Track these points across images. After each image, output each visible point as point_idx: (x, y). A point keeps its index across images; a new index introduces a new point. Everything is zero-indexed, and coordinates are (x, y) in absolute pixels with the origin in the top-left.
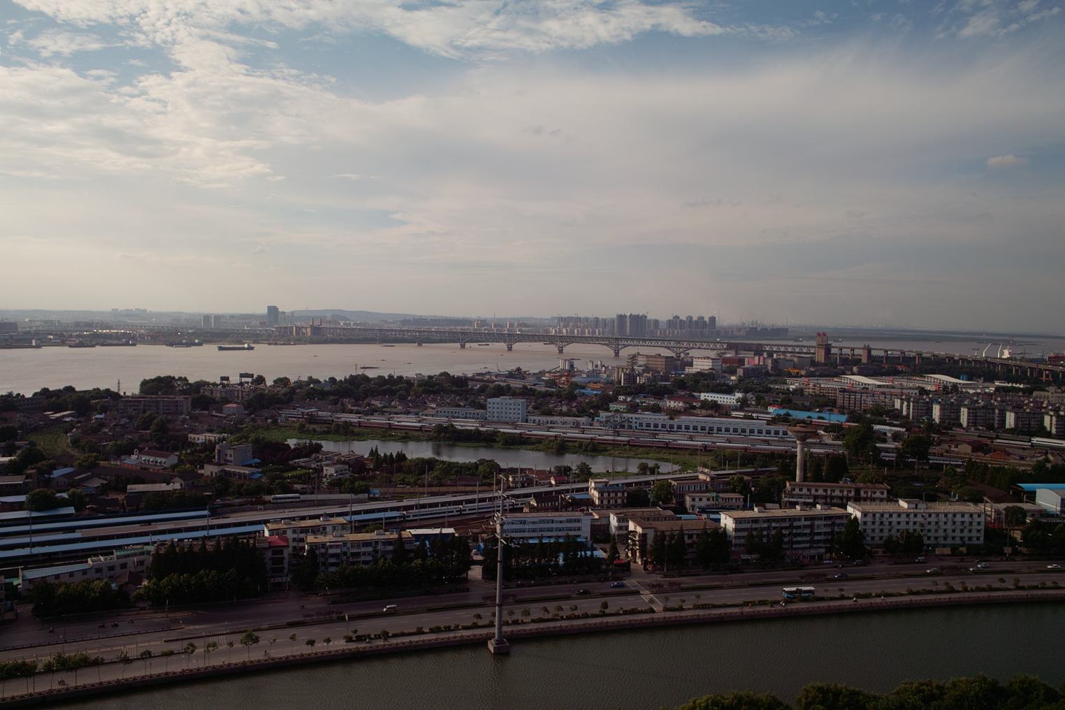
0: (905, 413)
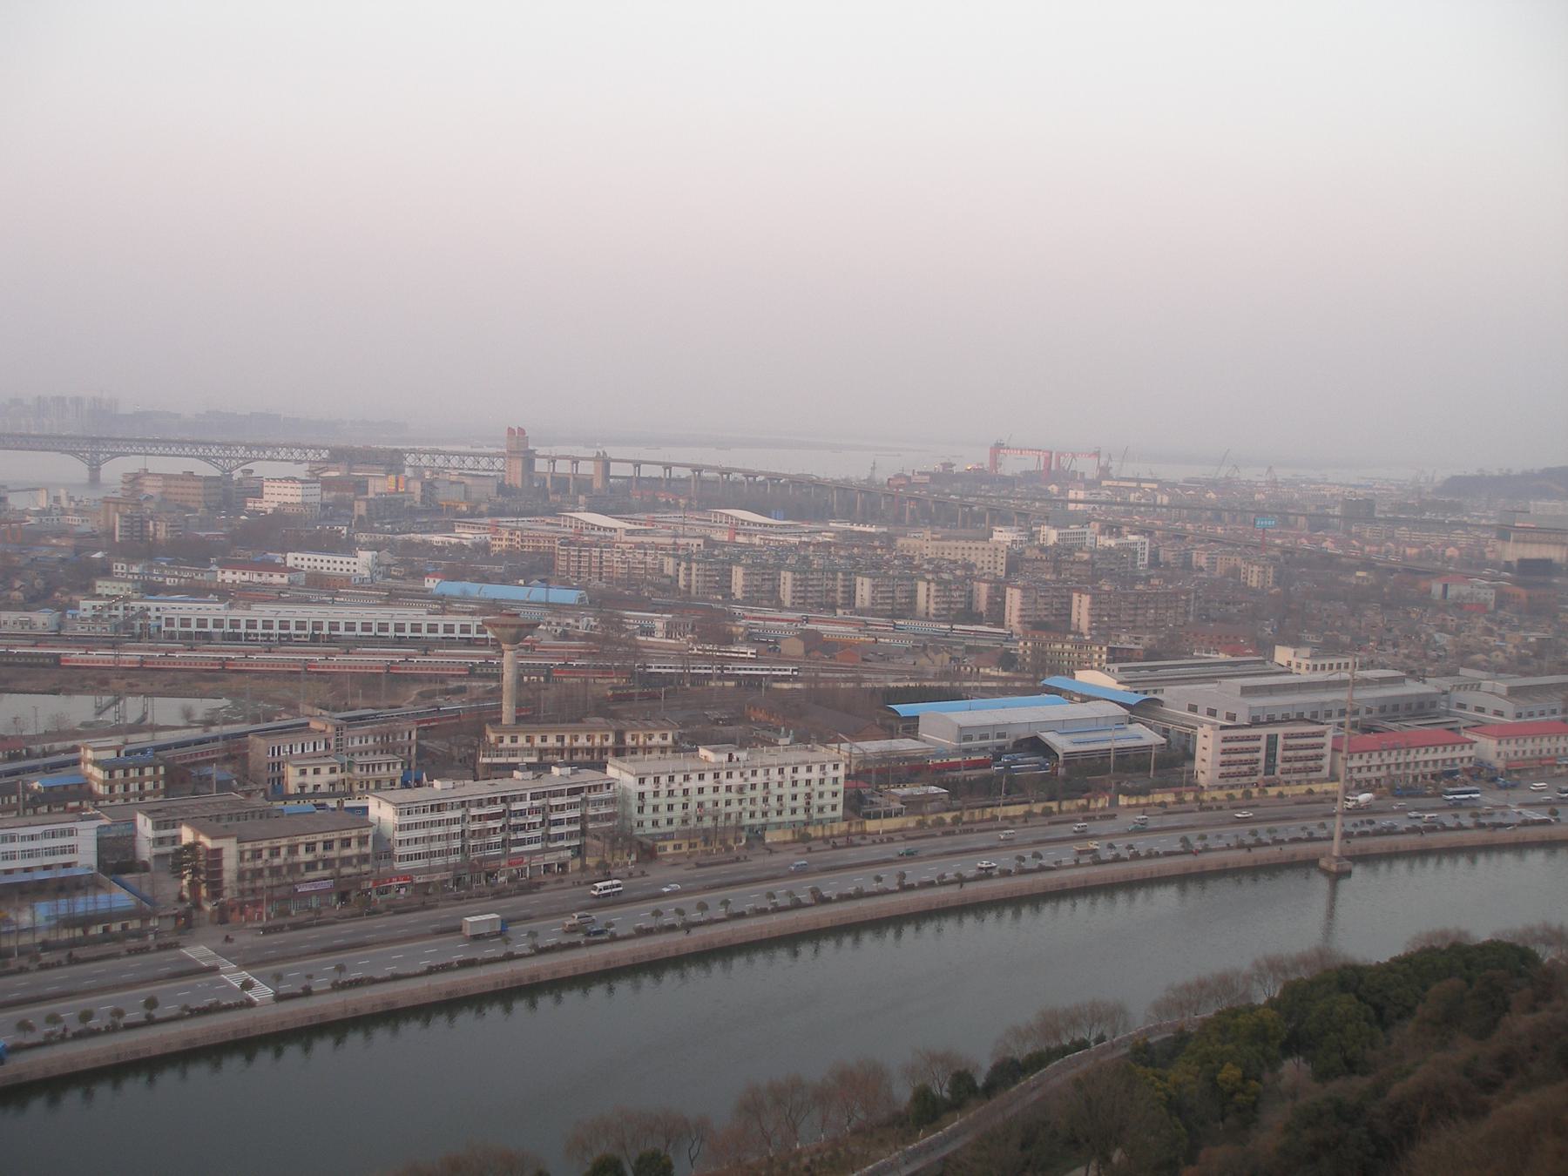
0: (682, 583)
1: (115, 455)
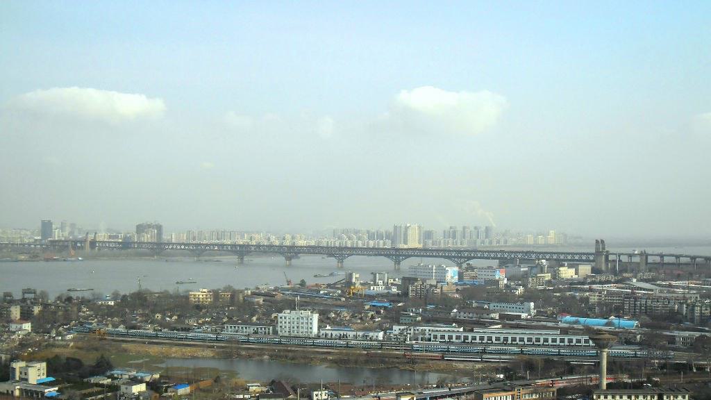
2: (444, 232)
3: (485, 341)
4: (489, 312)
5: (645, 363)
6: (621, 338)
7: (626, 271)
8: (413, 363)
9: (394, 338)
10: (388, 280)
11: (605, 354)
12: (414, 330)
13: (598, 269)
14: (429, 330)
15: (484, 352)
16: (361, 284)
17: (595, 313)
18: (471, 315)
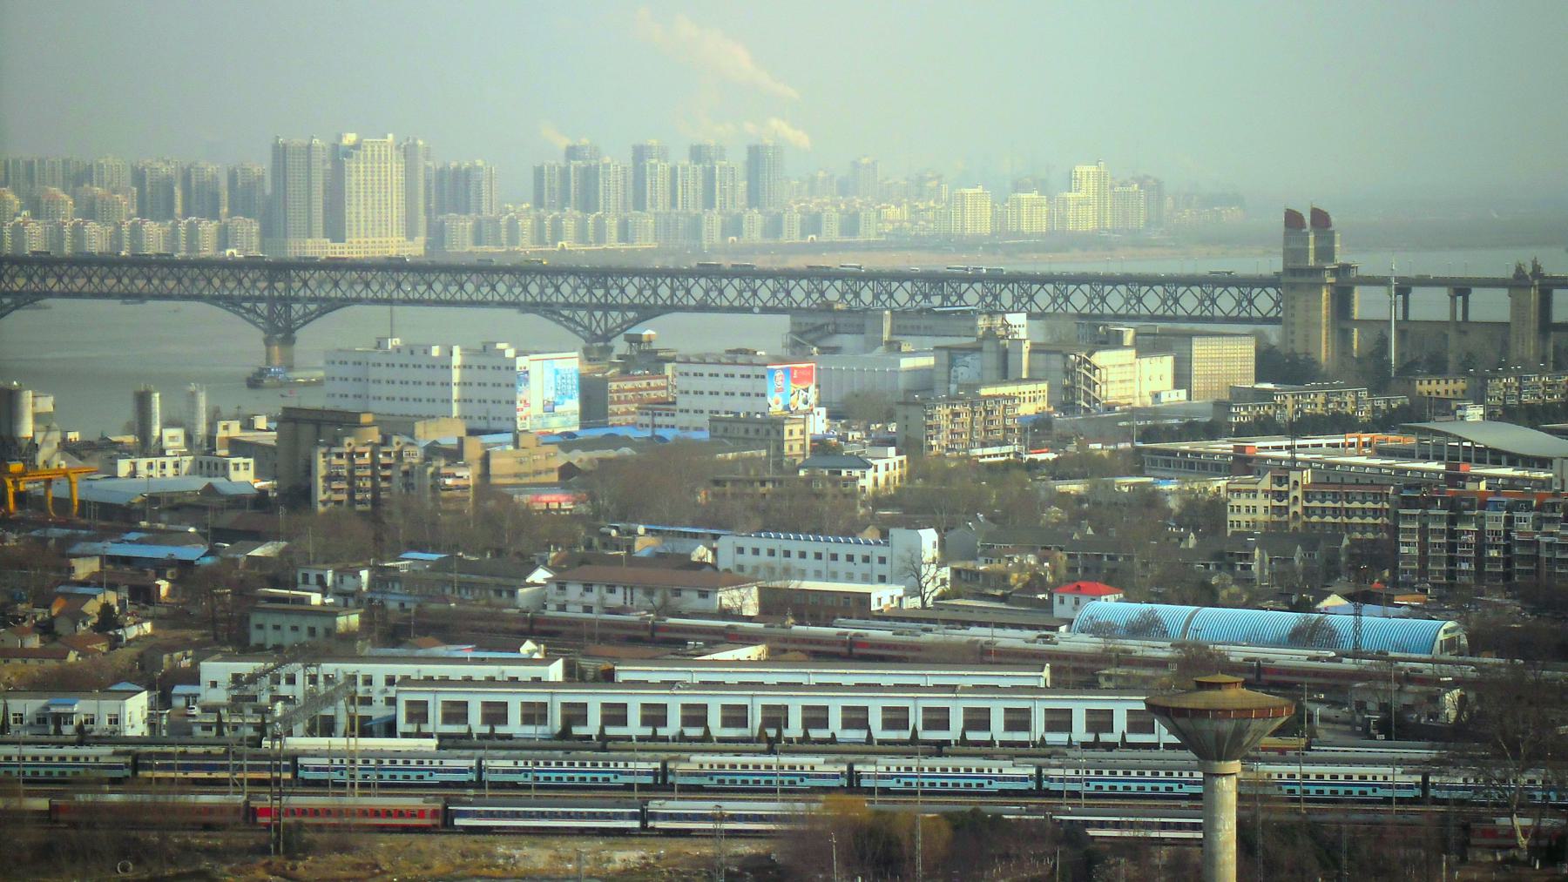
1: (330, 305)
2: (539, 173)
3: (674, 726)
4: (712, 577)
5: (1466, 828)
6: (1361, 706)
7: (1438, 368)
8: (290, 854)
9: (207, 727)
10: (212, 425)
11: (1228, 789)
12: (313, 679)
13: (1293, 356)
14: (390, 681)
15: (662, 784)
16: (66, 447)
17: (1246, 581)
18: (616, 599)
